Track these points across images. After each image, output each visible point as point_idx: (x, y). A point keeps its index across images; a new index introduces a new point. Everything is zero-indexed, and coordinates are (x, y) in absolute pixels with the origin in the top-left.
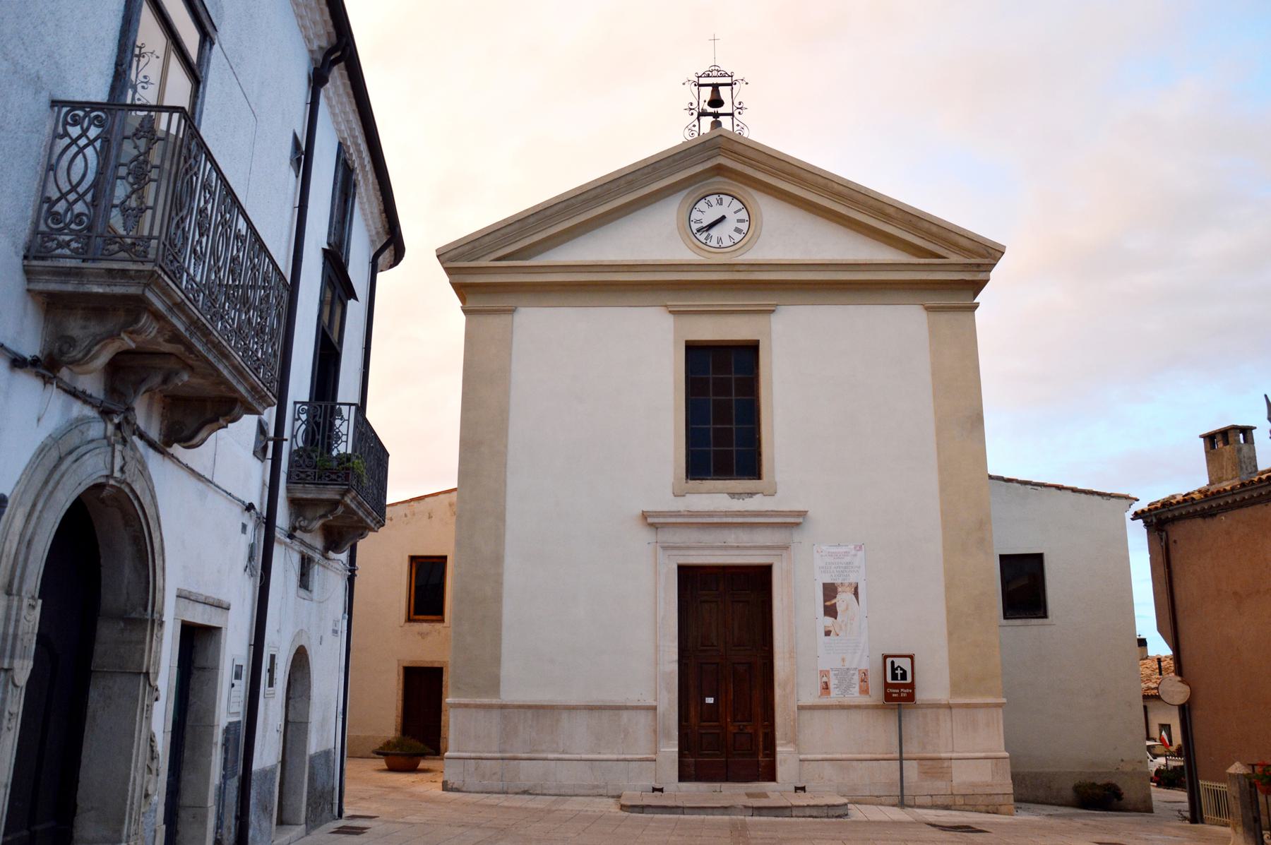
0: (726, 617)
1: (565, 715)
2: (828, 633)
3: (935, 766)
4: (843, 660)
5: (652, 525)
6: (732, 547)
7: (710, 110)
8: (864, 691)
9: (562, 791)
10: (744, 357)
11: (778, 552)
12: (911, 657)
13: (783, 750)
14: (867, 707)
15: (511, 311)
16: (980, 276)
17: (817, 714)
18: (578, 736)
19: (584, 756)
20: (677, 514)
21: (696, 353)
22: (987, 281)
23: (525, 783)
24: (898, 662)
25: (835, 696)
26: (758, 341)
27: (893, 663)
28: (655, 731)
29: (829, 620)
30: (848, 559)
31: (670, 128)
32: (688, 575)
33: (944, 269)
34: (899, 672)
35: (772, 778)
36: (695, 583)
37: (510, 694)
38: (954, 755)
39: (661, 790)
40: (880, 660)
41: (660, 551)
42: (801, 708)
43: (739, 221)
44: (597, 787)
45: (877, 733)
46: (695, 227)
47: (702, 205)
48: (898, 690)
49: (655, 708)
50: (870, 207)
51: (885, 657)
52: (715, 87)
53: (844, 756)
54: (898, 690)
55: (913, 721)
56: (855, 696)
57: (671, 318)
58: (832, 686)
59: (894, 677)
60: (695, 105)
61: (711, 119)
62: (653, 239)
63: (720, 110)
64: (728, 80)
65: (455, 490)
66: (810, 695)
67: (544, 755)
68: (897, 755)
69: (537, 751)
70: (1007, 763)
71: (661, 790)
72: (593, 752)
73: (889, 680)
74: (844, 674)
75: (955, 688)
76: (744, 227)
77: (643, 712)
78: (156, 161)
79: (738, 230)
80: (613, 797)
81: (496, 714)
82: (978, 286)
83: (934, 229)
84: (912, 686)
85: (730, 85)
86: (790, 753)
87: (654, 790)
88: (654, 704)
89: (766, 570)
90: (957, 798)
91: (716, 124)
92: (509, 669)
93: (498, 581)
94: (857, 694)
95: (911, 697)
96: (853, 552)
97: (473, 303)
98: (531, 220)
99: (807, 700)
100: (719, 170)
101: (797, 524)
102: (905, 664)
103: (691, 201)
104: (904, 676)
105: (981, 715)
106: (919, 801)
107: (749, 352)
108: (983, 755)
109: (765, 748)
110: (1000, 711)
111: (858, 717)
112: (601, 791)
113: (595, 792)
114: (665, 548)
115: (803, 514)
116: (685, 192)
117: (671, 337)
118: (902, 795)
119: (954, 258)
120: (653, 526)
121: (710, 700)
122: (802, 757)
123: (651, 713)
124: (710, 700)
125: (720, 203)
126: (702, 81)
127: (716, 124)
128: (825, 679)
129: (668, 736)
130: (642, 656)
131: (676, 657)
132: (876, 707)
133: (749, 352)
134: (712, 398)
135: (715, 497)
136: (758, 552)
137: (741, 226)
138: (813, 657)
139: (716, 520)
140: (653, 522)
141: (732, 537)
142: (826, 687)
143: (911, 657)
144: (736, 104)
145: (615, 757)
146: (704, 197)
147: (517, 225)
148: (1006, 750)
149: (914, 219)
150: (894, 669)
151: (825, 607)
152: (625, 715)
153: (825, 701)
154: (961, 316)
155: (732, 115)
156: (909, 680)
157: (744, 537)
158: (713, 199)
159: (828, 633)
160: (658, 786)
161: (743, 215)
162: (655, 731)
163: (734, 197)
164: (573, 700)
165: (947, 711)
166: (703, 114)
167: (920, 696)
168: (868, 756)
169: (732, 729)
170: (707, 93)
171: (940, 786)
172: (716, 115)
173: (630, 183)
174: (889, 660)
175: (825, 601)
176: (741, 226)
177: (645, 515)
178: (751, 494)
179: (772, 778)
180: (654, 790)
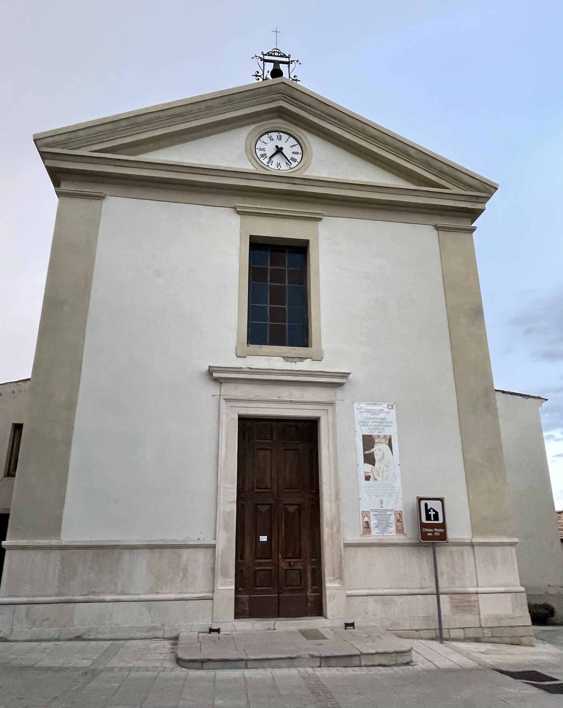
0: (280, 465)
1: (126, 555)
2: (368, 478)
3: (465, 601)
4: (381, 502)
5: (217, 380)
8: (400, 530)
9: (118, 635)
12: (442, 500)
13: (331, 585)
14: (403, 545)
15: (101, 198)
16: (479, 206)
17: (360, 551)
18: (138, 573)
19: (142, 597)
20: (238, 370)
21: (258, 246)
22: (483, 210)
23: (78, 628)
24: (431, 504)
25: (375, 535)
26: (308, 241)
27: (426, 505)
28: (213, 570)
29: (368, 467)
30: (382, 415)
31: (244, 74)
32: (249, 427)
33: (447, 200)
34: (432, 513)
36: (252, 430)
37: (66, 538)
38: (480, 590)
40: (415, 501)
41: (223, 402)
42: (347, 545)
44: (154, 628)
45: (414, 569)
47: (265, 138)
48: (430, 531)
49: (213, 547)
50: (397, 148)
51: (420, 499)
53: (385, 591)
54: (430, 531)
55: (444, 556)
56: (392, 535)
58: (372, 525)
59: (428, 517)
62: (226, 153)
64: (287, 60)
66: (353, 535)
67: (101, 597)
68: (441, 597)
69: (94, 593)
70: (524, 595)
72: (151, 592)
73: (424, 520)
74: (381, 513)
75: (475, 529)
76: (298, 158)
78: (385, 534)
80: (169, 639)
81: (56, 556)
82: (474, 214)
83: (445, 168)
84: (443, 526)
85: (288, 63)
86: (337, 589)
87: (211, 630)
88: (213, 542)
90: (486, 631)
93: (70, 427)
94: (394, 533)
95: (443, 537)
96: (386, 410)
97: (65, 187)
98: (123, 123)
100: (280, 113)
101: (340, 385)
102: (435, 505)
103: (258, 133)
104: (436, 517)
105: (498, 551)
106: (453, 634)
108: (503, 589)
109: (313, 584)
110: (513, 549)
111: (394, 552)
112: (159, 634)
113: (150, 634)
114: (227, 400)
115: (345, 375)
116: (253, 126)
117: (237, 231)
118: (441, 629)
120: (217, 380)
121: (264, 539)
122: (349, 592)
123: (210, 551)
124: (264, 539)
125: (280, 138)
126: (266, 58)
128: (366, 519)
129: (225, 575)
130: (206, 499)
131: (235, 498)
132: (411, 545)
133: (300, 250)
134: (269, 284)
135: (271, 359)
137: (295, 156)
138: (357, 499)
140: (215, 376)
141: (285, 393)
142: (367, 526)
143: (442, 500)
145: (173, 596)
146: (267, 133)
147: (110, 126)
148: (523, 586)
149: (430, 159)
150: (427, 511)
151: (365, 456)
152: (185, 553)
153: (366, 539)
154: (462, 236)
156: (441, 521)
157: (297, 394)
158: (274, 135)
159: (368, 478)
160: (215, 627)
161: (298, 149)
162: (213, 570)
163: (290, 135)
164: (134, 539)
165: (469, 548)
167: (451, 535)
168: (406, 591)
169: (283, 565)
170: (270, 67)
171: (470, 619)
173: (210, 108)
174: (423, 503)
175: (364, 450)
176: (295, 156)
178: (302, 359)
180: (211, 630)
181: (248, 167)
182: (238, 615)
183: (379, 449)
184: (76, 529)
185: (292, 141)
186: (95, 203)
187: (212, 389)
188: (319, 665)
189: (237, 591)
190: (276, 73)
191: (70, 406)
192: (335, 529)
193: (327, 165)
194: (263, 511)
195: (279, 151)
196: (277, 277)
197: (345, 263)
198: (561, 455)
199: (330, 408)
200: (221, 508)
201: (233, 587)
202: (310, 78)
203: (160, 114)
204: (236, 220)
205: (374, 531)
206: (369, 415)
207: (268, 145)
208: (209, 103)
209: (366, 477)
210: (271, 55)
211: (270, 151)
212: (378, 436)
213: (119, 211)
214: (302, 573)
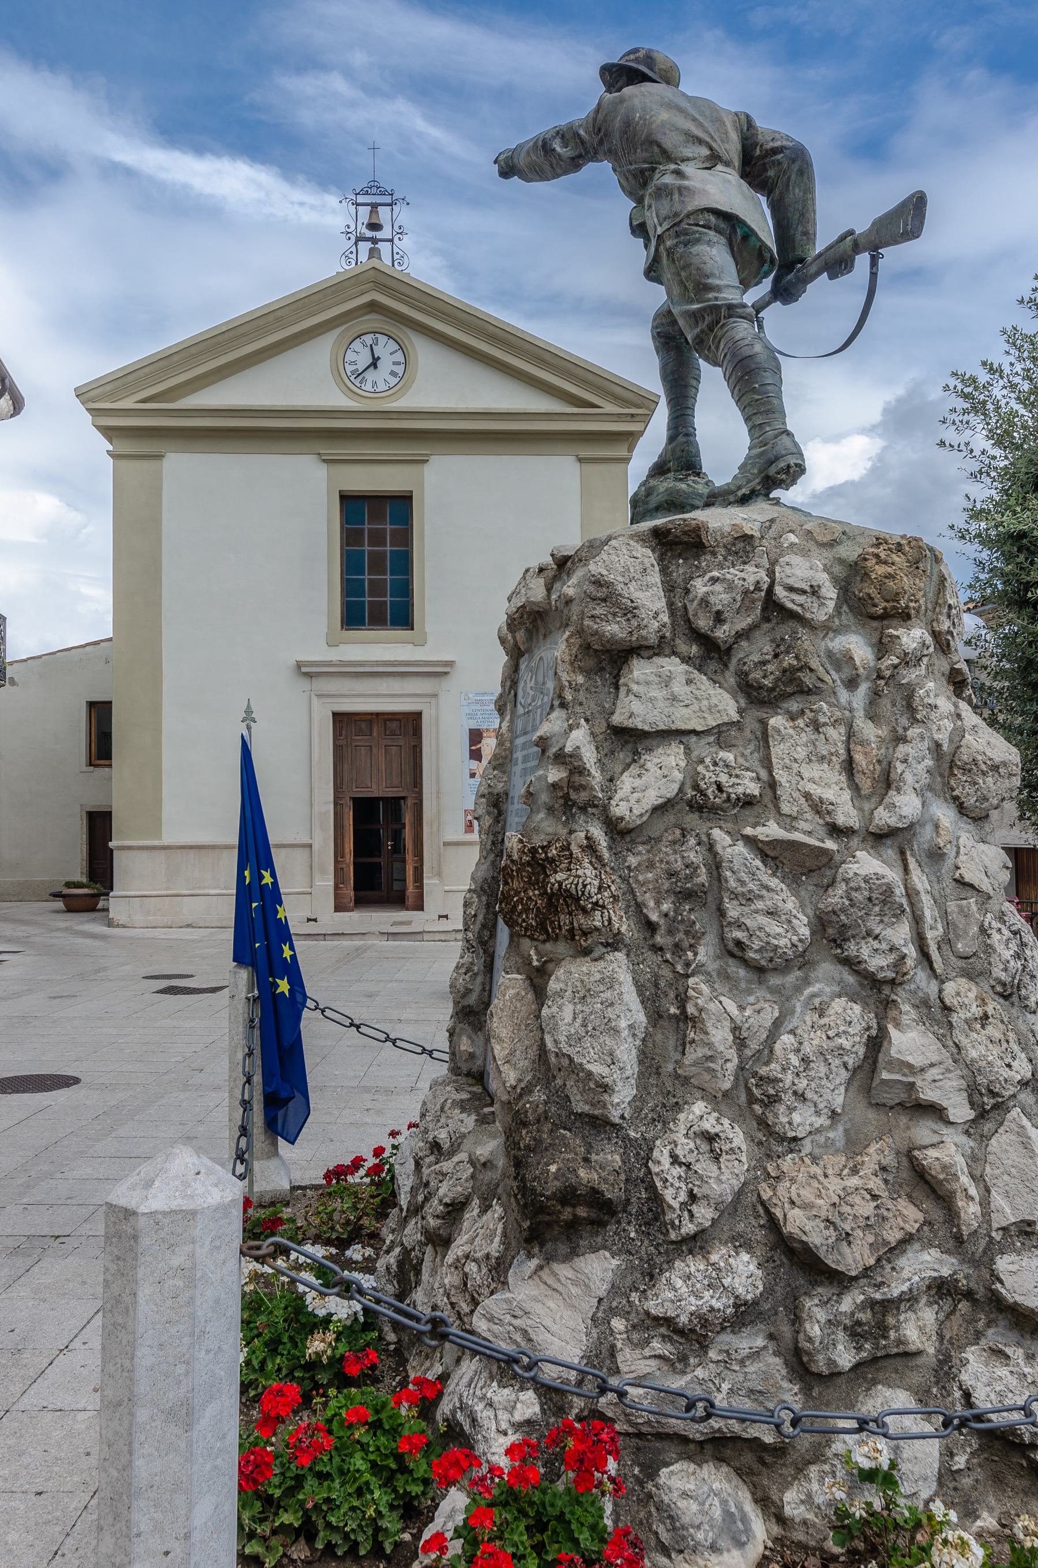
6: (384, 695)
7: (369, 234)
10: (356, 614)
11: (428, 700)
15: (159, 457)
20: (330, 664)
35: (421, 908)
37: (167, 840)
39: (315, 920)
41: (315, 699)
42: (446, 844)
43: (394, 363)
46: (349, 368)
47: (357, 345)
49: (310, 846)
52: (374, 206)
57: (324, 467)
60: (353, 228)
61: (369, 245)
62: (305, 382)
63: (379, 235)
64: (387, 199)
65: (110, 640)
67: (206, 891)
69: (199, 888)
71: (315, 920)
76: (399, 370)
77: (300, 850)
79: (393, 374)
87: (309, 920)
88: (309, 841)
89: (417, 716)
91: (373, 253)
92: (170, 811)
99: (451, 837)
100: (373, 307)
101: (446, 673)
107: (356, 614)
114: (319, 696)
115: (450, 664)
119: (609, 408)
120: (309, 675)
123: (307, 850)
126: (361, 199)
127: (373, 253)
129: (323, 871)
131: (332, 798)
133: (401, 505)
136: (409, 700)
137: (396, 368)
139: (367, 669)
140: (306, 672)
141: (384, 686)
144: (396, 228)
146: (359, 336)
154: (621, 466)
155: (391, 241)
161: (399, 357)
163: (390, 337)
166: (359, 239)
172: (374, 241)
176: (396, 368)
177: (299, 665)
179: (421, 908)
180: (309, 920)
181: (343, 402)
187: (305, 684)
188: (784, 436)
192: (435, 829)
193: (441, 385)
194: (607, 165)
196: (377, 538)
199: (433, 701)
200: (316, 809)
201: (332, 883)
203: (220, 338)
204: (321, 472)
206: (478, 707)
208: (279, 314)
210: (367, 193)
212: (487, 730)
213: (181, 467)
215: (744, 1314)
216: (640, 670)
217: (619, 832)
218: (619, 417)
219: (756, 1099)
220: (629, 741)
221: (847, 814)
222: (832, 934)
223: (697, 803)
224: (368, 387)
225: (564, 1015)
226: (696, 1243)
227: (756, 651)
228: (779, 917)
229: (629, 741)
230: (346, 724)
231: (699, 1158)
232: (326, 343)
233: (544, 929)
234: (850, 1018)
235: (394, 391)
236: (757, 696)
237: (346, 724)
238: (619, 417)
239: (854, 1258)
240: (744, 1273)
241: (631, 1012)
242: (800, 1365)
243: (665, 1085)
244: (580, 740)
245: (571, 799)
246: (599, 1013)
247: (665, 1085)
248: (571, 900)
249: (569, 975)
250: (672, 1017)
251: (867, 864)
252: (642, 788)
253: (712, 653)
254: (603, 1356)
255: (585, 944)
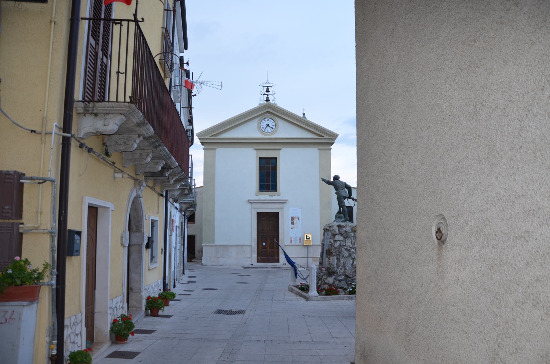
0: (268, 226)
5: (251, 203)
15: (215, 149)
20: (256, 200)
24: (308, 235)
25: (293, 243)
29: (292, 226)
37: (217, 243)
52: (268, 87)
61: (266, 96)
62: (250, 131)
76: (274, 127)
89: (278, 213)
92: (217, 237)
100: (268, 112)
119: (327, 137)
120: (251, 203)
121: (264, 244)
124: (264, 244)
125: (268, 120)
126: (264, 85)
130: (249, 234)
135: (266, 196)
142: (291, 241)
152: (244, 247)
153: (291, 244)
158: (266, 119)
161: (274, 124)
164: (232, 244)
166: (264, 94)
169: (269, 250)
172: (268, 95)
177: (249, 201)
181: (259, 135)
182: (258, 262)
183: (296, 221)
184: (219, 241)
185: (272, 121)
186: (212, 151)
187: (250, 205)
189: (257, 257)
190: (268, 100)
191: (213, 211)
193: (285, 131)
195: (268, 125)
197: (289, 163)
198: (2, 323)
202: (280, 100)
205: (293, 242)
207: (264, 123)
209: (329, 291)
211: (265, 126)
213: (221, 152)
214: (274, 252)
215: (343, 280)
216: (336, 236)
217: (335, 248)
218: (329, 139)
219: (344, 266)
220: (336, 241)
221: (351, 246)
222: (350, 255)
223: (340, 246)
224: (266, 131)
225: (331, 260)
226: (340, 275)
227: (345, 234)
228: (346, 254)
229: (336, 241)
230: (260, 215)
231: (341, 270)
232: (257, 120)
233: (330, 255)
234: (351, 261)
235: (272, 133)
236: (345, 238)
237: (260, 215)
238: (329, 139)
239: (351, 276)
240: (343, 277)
241: (336, 260)
242: (347, 284)
243: (338, 266)
244: (332, 241)
245: (331, 245)
246: (334, 260)
247: (338, 266)
248: (332, 253)
249: (331, 258)
250: (338, 260)
251: (352, 250)
252: (337, 245)
253: (341, 235)
254: (334, 283)
255: (332, 256)
